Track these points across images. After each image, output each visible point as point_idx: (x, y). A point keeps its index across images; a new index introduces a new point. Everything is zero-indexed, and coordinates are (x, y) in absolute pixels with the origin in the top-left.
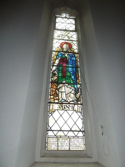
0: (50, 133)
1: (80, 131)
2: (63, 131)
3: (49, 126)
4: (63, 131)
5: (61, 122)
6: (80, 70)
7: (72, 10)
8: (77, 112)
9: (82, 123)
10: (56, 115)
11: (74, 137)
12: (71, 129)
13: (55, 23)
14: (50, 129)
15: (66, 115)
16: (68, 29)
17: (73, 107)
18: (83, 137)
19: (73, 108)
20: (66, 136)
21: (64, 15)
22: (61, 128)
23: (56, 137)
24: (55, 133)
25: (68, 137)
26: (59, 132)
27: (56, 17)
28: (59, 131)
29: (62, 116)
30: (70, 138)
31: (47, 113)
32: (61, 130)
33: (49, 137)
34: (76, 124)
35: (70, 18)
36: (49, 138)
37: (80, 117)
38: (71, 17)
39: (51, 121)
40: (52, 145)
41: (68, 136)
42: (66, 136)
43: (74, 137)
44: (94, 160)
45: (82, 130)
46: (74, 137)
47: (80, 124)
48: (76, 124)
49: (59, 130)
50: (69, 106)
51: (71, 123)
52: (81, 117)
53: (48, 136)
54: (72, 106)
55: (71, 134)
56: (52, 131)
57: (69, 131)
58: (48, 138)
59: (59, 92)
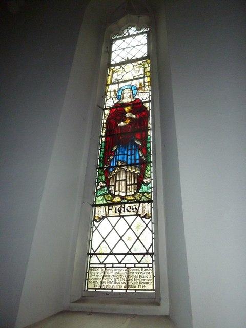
0: (94, 260)
1: (147, 253)
2: (133, 254)
3: (92, 248)
4: (133, 254)
5: (112, 239)
6: (154, 137)
7: (139, 17)
8: (141, 218)
9: (92, 241)
10: (104, 227)
11: (135, 264)
12: (111, 250)
13: (109, 52)
14: (130, 252)
15: (122, 226)
16: (134, 58)
17: (136, 208)
18: (91, 266)
19: (137, 209)
20: (120, 263)
21: (133, 31)
22: (130, 250)
23: (103, 266)
24: (120, 258)
25: (124, 265)
26: (109, 256)
27: (111, 42)
28: (126, 254)
29: (128, 227)
30: (128, 268)
31: (88, 224)
32: (111, 254)
33: (91, 266)
34: (140, 240)
35: (138, 34)
36: (107, 267)
37: (147, 226)
38: (141, 31)
39: (96, 240)
40: (95, 280)
41: (125, 264)
42: (120, 263)
43: (136, 265)
44: (164, 309)
45: (150, 251)
46: (136, 265)
47: (147, 238)
48: (140, 240)
49: (126, 252)
50: (129, 208)
51: (130, 237)
52: (150, 226)
53: (90, 264)
54: (134, 207)
55: (130, 259)
56: (113, 256)
57: (144, 254)
58: (90, 267)
59: (128, 187)
